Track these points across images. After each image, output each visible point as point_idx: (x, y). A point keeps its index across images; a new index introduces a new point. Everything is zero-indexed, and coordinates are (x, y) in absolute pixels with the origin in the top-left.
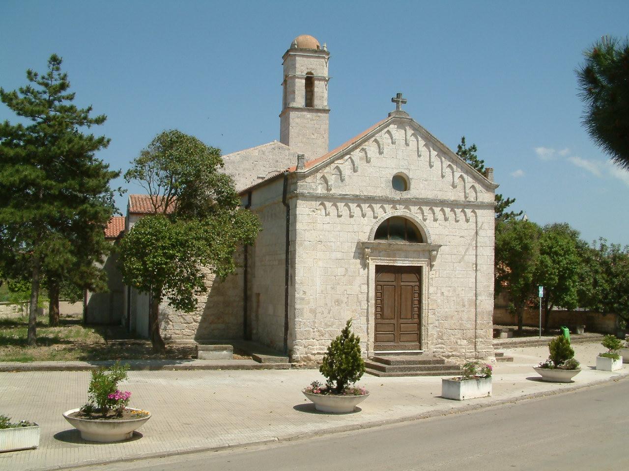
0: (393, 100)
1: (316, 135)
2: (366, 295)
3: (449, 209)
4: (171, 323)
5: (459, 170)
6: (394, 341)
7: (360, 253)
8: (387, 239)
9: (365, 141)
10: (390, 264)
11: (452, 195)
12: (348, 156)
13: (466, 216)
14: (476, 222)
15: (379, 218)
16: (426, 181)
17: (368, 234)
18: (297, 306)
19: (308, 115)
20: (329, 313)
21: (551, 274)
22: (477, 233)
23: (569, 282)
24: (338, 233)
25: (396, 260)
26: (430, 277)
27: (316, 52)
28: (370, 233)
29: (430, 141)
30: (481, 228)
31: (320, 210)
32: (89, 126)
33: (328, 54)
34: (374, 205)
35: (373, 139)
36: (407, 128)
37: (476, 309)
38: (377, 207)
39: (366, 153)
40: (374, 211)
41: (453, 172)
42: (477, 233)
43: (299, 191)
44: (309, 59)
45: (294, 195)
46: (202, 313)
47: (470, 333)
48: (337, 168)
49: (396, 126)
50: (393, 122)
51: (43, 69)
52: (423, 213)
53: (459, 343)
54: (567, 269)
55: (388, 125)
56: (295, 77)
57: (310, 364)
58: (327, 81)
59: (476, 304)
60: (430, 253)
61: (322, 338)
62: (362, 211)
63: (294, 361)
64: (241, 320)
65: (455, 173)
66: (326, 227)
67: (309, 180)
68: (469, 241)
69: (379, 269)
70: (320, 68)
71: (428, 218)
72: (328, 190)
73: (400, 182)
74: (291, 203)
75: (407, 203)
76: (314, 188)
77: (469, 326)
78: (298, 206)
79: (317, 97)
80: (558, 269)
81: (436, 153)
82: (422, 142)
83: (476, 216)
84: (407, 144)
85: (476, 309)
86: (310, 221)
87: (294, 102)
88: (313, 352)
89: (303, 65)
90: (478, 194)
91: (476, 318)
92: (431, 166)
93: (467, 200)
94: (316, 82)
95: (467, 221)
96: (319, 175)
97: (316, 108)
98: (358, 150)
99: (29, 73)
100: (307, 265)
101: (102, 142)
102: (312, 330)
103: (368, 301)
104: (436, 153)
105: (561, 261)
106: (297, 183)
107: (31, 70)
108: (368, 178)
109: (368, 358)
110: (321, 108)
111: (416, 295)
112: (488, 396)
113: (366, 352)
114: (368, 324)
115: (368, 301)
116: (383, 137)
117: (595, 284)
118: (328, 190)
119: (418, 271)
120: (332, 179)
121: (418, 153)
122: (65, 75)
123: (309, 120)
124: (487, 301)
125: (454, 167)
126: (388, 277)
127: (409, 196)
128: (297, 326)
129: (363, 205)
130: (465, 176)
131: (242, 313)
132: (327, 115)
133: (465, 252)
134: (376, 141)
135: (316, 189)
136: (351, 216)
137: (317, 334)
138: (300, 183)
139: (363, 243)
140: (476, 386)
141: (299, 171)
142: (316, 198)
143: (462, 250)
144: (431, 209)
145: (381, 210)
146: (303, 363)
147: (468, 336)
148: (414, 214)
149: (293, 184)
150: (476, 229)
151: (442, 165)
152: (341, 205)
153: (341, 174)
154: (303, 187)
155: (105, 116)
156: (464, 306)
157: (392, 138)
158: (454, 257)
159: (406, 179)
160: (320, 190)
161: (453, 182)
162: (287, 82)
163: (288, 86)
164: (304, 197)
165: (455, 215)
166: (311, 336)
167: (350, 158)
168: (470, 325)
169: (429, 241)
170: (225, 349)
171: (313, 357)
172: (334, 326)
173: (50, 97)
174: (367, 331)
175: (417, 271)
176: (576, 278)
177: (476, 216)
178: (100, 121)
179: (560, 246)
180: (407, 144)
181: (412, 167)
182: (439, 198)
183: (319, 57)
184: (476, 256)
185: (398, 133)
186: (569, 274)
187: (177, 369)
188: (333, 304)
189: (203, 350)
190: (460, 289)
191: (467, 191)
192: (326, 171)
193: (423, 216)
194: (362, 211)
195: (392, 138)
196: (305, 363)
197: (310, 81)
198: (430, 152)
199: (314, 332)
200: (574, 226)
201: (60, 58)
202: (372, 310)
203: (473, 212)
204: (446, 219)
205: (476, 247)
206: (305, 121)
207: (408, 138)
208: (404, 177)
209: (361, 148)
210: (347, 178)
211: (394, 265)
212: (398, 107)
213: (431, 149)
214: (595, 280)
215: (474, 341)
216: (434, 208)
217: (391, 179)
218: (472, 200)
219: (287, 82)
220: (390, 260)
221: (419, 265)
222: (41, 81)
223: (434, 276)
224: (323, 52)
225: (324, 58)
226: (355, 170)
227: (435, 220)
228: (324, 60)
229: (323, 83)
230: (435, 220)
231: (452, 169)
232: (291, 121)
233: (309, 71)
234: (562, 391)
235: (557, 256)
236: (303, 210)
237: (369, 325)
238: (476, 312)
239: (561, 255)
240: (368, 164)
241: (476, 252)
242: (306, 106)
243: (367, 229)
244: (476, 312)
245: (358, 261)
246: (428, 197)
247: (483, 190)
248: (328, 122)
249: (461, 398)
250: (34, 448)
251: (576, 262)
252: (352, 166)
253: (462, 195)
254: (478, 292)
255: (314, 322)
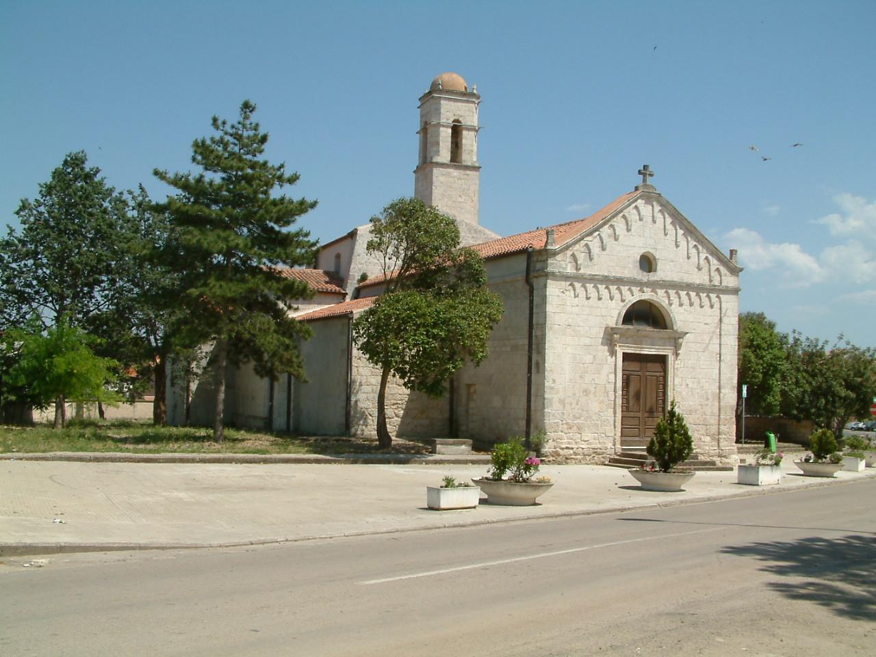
0: (640, 172)
1: (464, 197)
2: (613, 386)
3: (695, 294)
4: (370, 417)
5: (705, 251)
6: (638, 436)
7: (608, 340)
8: (632, 325)
9: (614, 217)
10: (637, 352)
11: (700, 278)
12: (597, 233)
13: (710, 301)
14: (721, 309)
15: (627, 301)
16: (673, 261)
17: (616, 319)
18: (546, 396)
19: (455, 173)
20: (577, 404)
21: (755, 371)
22: (721, 320)
23: (773, 380)
24: (586, 317)
25: (643, 348)
26: (676, 367)
27: (464, 94)
28: (618, 317)
29: (676, 218)
30: (725, 315)
31: (569, 291)
32: (281, 186)
33: (478, 97)
34: (622, 287)
35: (621, 215)
36: (655, 203)
37: (719, 402)
38: (625, 289)
39: (614, 230)
40: (621, 294)
41: (698, 253)
42: (721, 320)
43: (550, 269)
44: (456, 104)
45: (543, 274)
46: (404, 406)
47: (714, 429)
48: (587, 245)
49: (644, 201)
50: (641, 197)
51: (232, 116)
52: (669, 297)
53: (703, 440)
54: (771, 365)
55: (636, 201)
56: (439, 125)
57: (559, 459)
58: (477, 131)
59: (719, 398)
60: (676, 341)
61: (570, 431)
62: (610, 293)
63: (543, 455)
64: (447, 415)
65: (701, 254)
66: (576, 310)
67: (559, 257)
68: (713, 329)
69: (626, 357)
70: (469, 114)
71: (674, 302)
72: (577, 269)
73: (647, 263)
74: (535, 282)
75: (654, 285)
76: (564, 266)
77: (712, 421)
78: (548, 286)
79: (465, 150)
80: (762, 365)
81: (682, 232)
82: (669, 220)
83: (720, 302)
84: (654, 221)
85: (719, 402)
86: (560, 303)
87: (438, 155)
88: (562, 446)
89: (449, 110)
90: (723, 278)
91: (719, 413)
92: (677, 246)
93: (712, 283)
94: (465, 133)
95: (712, 306)
96: (569, 253)
97: (464, 164)
98: (607, 226)
99: (215, 120)
100: (556, 351)
101: (303, 207)
102: (561, 422)
103: (615, 391)
104: (682, 232)
105: (765, 356)
106: (547, 260)
107: (217, 116)
108: (616, 257)
109: (615, 453)
110: (469, 164)
111: (661, 386)
112: (778, 483)
113: (613, 447)
114: (615, 416)
115: (615, 391)
116: (631, 213)
117: (797, 383)
118: (577, 269)
119: (662, 360)
120: (581, 258)
121: (665, 232)
122: (257, 125)
123: (456, 179)
124: (731, 395)
125: (700, 248)
126: (634, 366)
127: (655, 278)
128: (546, 418)
129: (611, 287)
130: (710, 257)
131: (448, 407)
132: (477, 173)
133: (710, 341)
134: (624, 217)
135: (566, 268)
136: (600, 299)
137: (565, 426)
138: (550, 261)
139: (612, 329)
140: (770, 471)
141: (549, 247)
142: (566, 278)
143: (707, 338)
144: (677, 293)
145: (629, 293)
146: (551, 459)
147: (712, 433)
148: (659, 297)
149: (541, 261)
150: (721, 317)
151: (688, 245)
152: (590, 286)
153: (590, 253)
154: (555, 265)
155: (298, 174)
156: (708, 399)
157: (639, 214)
158: (698, 345)
159: (652, 259)
160: (570, 270)
161: (699, 264)
162: (427, 131)
163: (429, 136)
164: (555, 276)
165: (700, 300)
166: (560, 429)
167: (599, 234)
168: (713, 421)
169: (675, 328)
170: (464, 443)
171: (561, 452)
172: (582, 418)
173: (240, 150)
174: (614, 425)
175: (662, 360)
176: (778, 376)
177: (720, 302)
178: (293, 180)
179: (763, 339)
180: (654, 221)
181: (659, 247)
182: (685, 281)
183: (468, 102)
184: (720, 345)
185: (646, 210)
186: (773, 371)
187: (427, 463)
188: (581, 394)
189: (441, 444)
190: (704, 380)
191: (712, 274)
192: (575, 249)
193: (669, 300)
194: (610, 293)
195: (639, 214)
196: (554, 459)
197: (457, 130)
198: (676, 230)
199: (562, 424)
200: (770, 317)
201: (254, 105)
202: (619, 401)
203: (718, 297)
204: (691, 304)
205: (720, 335)
206: (451, 180)
207: (655, 215)
208: (650, 257)
209: (609, 224)
210: (595, 257)
211: (642, 352)
212: (644, 181)
213: (678, 227)
214: (797, 378)
215: (717, 437)
216: (680, 292)
217: (639, 259)
218: (717, 284)
219: (427, 131)
220: (638, 347)
221: (664, 354)
222: (231, 131)
223: (679, 366)
224: (473, 95)
225: (474, 102)
226: (603, 249)
227: (681, 305)
228: (473, 105)
229: (473, 133)
230: (681, 305)
231: (698, 249)
232: (434, 179)
233: (456, 118)
234: (821, 484)
235: (760, 349)
236: (554, 290)
237: (617, 418)
238: (720, 405)
239: (764, 349)
240: (616, 242)
241: (720, 341)
242: (451, 161)
243: (615, 314)
244: (720, 405)
245: (606, 348)
246: (675, 280)
247: (728, 273)
248: (477, 182)
249: (760, 484)
250: (475, 507)
251: (781, 358)
252: (600, 243)
253: (707, 278)
254: (722, 384)
255: (563, 413)
